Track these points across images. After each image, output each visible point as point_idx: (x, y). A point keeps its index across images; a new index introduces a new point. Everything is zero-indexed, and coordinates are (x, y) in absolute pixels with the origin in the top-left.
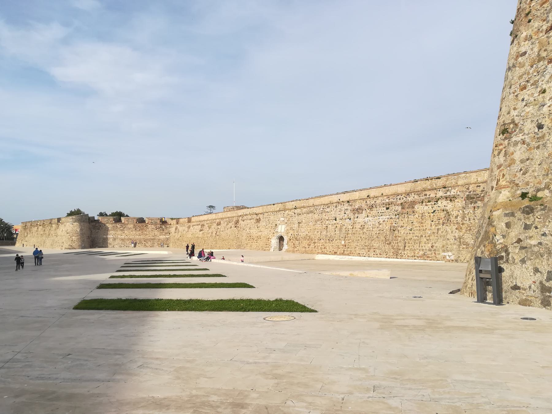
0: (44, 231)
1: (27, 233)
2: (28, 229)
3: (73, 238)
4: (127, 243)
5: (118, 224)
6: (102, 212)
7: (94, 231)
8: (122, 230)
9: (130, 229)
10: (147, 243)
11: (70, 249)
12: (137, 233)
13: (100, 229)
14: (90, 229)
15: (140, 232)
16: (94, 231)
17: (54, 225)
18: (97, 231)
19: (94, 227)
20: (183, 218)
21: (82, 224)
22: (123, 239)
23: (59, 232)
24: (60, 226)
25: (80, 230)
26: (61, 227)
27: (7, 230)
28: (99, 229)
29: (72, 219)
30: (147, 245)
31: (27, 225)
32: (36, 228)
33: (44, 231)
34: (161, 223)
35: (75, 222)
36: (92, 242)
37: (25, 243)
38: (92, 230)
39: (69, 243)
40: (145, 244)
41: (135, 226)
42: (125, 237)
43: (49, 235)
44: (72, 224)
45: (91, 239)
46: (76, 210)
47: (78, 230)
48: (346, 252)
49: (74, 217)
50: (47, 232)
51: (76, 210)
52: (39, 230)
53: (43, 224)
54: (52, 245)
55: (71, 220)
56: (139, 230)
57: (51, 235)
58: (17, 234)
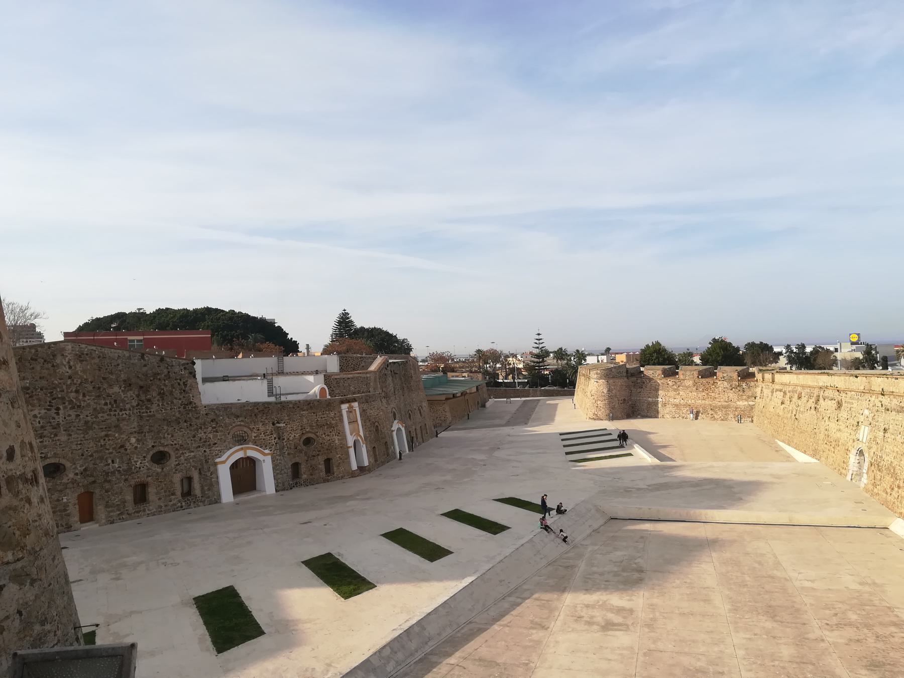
4: (684, 411)
5: (669, 380)
7: (634, 390)
8: (675, 390)
9: (688, 387)
12: (700, 395)
13: (644, 387)
14: (628, 387)
15: (704, 394)
16: (634, 390)
18: (639, 390)
19: (635, 384)
21: (611, 381)
22: (677, 405)
25: (608, 391)
30: (716, 416)
34: (739, 378)
35: (601, 378)
38: (632, 389)
39: (593, 411)
40: (712, 414)
41: (695, 384)
44: (597, 382)
46: (654, 343)
47: (605, 391)
51: (654, 343)
56: (703, 389)
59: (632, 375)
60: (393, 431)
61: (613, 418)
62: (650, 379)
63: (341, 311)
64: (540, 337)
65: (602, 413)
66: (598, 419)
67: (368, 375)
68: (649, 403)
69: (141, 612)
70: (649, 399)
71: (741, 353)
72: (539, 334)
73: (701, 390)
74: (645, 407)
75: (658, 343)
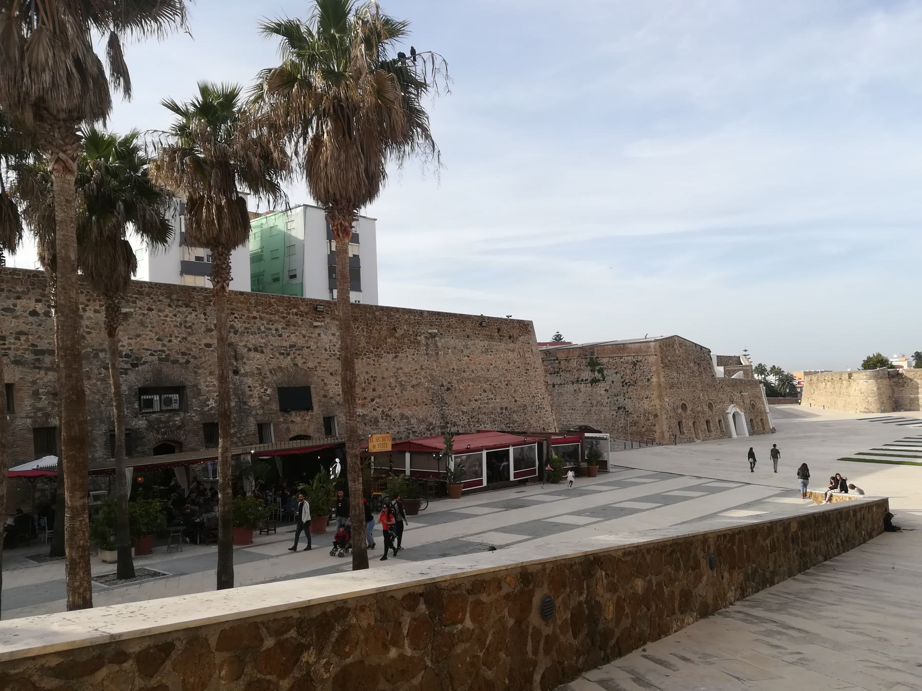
0: (834, 388)
1: (814, 390)
2: (815, 385)
6: (919, 351)
11: (867, 413)
13: (906, 386)
14: (891, 386)
16: (896, 389)
17: (844, 382)
18: (901, 388)
19: (897, 384)
20: (502, 543)
21: (879, 381)
23: (852, 392)
24: (852, 383)
25: (878, 389)
26: (854, 385)
27: (788, 383)
29: (866, 375)
31: (813, 379)
32: (824, 383)
33: (834, 388)
35: (870, 378)
36: (896, 403)
37: (812, 402)
38: (894, 388)
39: (864, 406)
43: (840, 394)
45: (893, 399)
46: (875, 355)
47: (875, 389)
48: (434, 435)
49: (868, 373)
50: (837, 390)
51: (875, 355)
52: (828, 386)
53: (832, 379)
54: (844, 406)
55: (865, 377)
57: (842, 393)
58: (801, 388)
59: (893, 377)
60: (728, 413)
61: (883, 411)
62: (911, 380)
63: (555, 333)
64: (747, 353)
65: (873, 407)
66: (869, 412)
67: (748, 368)
68: (911, 399)
69: (776, 472)
70: (912, 396)
71: (198, 520)
72: (746, 351)
74: (907, 402)
75: (879, 355)
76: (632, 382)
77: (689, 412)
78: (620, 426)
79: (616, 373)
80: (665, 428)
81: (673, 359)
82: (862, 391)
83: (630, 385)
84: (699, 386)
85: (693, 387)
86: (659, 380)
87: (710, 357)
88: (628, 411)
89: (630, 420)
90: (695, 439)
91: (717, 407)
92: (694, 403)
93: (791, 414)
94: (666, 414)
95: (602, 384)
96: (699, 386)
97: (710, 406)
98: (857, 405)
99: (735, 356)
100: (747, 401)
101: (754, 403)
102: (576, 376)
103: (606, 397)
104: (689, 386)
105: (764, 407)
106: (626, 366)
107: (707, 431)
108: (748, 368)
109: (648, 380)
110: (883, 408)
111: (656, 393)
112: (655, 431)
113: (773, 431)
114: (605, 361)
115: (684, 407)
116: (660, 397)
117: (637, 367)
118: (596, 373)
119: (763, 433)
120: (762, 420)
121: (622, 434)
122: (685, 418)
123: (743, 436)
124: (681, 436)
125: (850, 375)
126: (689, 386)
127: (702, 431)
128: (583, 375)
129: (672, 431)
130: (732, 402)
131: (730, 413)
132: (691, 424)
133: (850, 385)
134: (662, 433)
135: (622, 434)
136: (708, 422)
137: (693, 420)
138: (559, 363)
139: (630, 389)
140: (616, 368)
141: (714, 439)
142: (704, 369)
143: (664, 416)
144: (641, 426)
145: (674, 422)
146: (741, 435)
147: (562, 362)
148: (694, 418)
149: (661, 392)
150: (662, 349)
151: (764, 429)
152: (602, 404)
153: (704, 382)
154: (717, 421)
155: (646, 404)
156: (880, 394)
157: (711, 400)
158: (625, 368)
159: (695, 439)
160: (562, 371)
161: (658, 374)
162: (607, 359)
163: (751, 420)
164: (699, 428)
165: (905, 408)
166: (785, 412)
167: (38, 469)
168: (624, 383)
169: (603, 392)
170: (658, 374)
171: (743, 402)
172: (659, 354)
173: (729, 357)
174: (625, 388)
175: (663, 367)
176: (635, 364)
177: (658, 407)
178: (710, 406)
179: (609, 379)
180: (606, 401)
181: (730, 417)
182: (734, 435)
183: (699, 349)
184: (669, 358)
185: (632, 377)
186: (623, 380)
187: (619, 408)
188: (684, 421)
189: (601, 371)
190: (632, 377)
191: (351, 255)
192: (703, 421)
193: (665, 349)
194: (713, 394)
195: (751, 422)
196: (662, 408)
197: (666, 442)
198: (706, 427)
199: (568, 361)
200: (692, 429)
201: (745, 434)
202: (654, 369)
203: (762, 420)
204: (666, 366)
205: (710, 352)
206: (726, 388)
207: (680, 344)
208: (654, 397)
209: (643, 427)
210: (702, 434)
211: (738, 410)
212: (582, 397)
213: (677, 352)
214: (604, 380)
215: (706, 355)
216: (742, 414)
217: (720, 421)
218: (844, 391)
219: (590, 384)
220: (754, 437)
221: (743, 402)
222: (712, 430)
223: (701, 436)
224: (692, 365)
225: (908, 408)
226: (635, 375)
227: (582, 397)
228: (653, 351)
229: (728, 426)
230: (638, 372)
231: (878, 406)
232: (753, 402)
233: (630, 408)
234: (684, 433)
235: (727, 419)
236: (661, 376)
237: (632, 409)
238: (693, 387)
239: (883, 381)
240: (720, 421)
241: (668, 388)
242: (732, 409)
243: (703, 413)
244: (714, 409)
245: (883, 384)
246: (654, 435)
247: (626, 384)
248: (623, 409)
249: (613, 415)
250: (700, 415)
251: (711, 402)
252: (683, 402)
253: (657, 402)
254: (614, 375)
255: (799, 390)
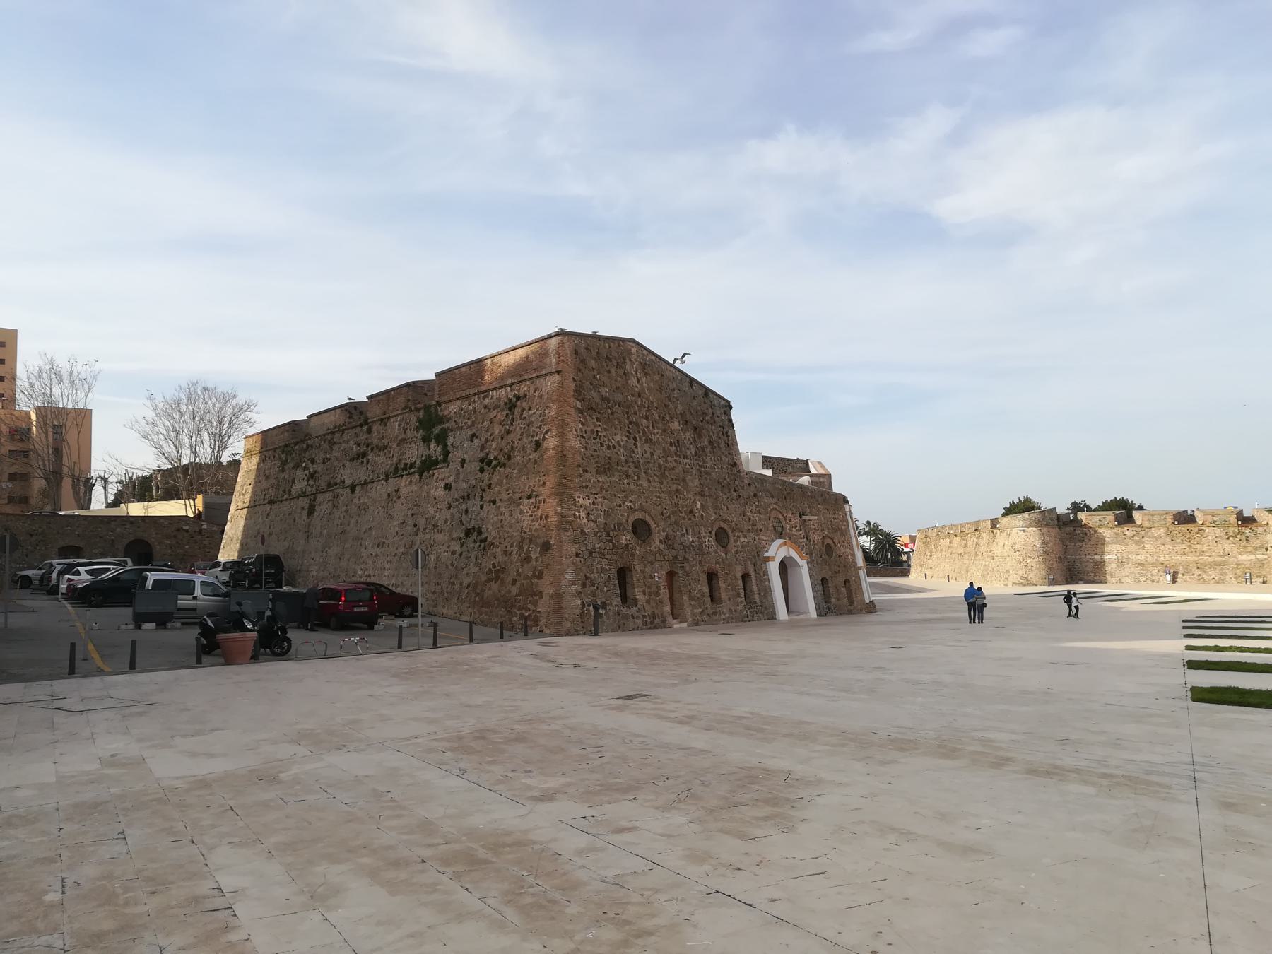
1: (931, 552)
2: (932, 544)
3: (1029, 561)
8: (1137, 543)
10: (1205, 572)
14: (1062, 540)
15: (1184, 546)
16: (1070, 545)
17: (984, 535)
18: (1079, 544)
19: (1072, 537)
21: (1045, 530)
23: (998, 548)
26: (1001, 537)
28: (1083, 541)
35: (1030, 525)
36: (1070, 570)
37: (929, 572)
38: (1068, 543)
39: (1021, 573)
40: (1199, 575)
42: (1147, 558)
43: (976, 555)
44: (1024, 531)
46: (1022, 499)
47: (1038, 543)
49: (1027, 516)
50: (970, 549)
51: (1022, 499)
52: (955, 544)
53: (962, 532)
55: (1021, 522)
60: (768, 559)
65: (1037, 573)
73: (1179, 541)
76: (501, 459)
77: (656, 543)
78: (466, 581)
79: (473, 437)
80: (569, 582)
81: (619, 397)
82: (1016, 547)
83: (496, 466)
84: (694, 483)
85: (676, 480)
86: (562, 442)
87: (730, 420)
88: (486, 539)
89: (487, 563)
90: (670, 619)
91: (739, 542)
92: (676, 523)
93: (902, 589)
94: (574, 541)
95: (441, 473)
96: (694, 483)
97: (721, 537)
98: (1008, 571)
99: (798, 460)
100: (817, 537)
101: (831, 542)
102: (395, 459)
103: (445, 505)
104: (663, 476)
105: (853, 555)
106: (492, 415)
107: (707, 599)
108: (822, 480)
109: (538, 445)
110: (1051, 577)
111: (551, 481)
112: (540, 594)
113: (871, 608)
114: (452, 409)
115: (641, 530)
116: (563, 491)
117: (517, 411)
118: (433, 445)
119: (850, 612)
120: (847, 581)
121: (466, 604)
122: (642, 559)
123: (801, 617)
124: (624, 610)
125: (994, 523)
126: (663, 476)
127: (691, 599)
128: (408, 453)
129: (593, 594)
130: (781, 535)
131: (773, 559)
132: (659, 577)
133: (994, 539)
134: (558, 597)
135: (466, 604)
136: (711, 577)
137: (667, 568)
138: (369, 431)
139: (496, 478)
140: (473, 425)
141: (726, 621)
142: (710, 442)
143: (570, 549)
144: (509, 580)
145: (604, 570)
146: (799, 613)
147: (375, 428)
148: (670, 562)
149: (564, 476)
150: (583, 361)
151: (852, 603)
152: (435, 526)
153: (707, 473)
154: (739, 576)
155: (526, 516)
156: (1047, 553)
157: (724, 521)
158: (491, 421)
159: (670, 619)
160: (372, 450)
161: (562, 427)
162: (458, 403)
163: (824, 581)
164: (685, 590)
165: (1085, 577)
166: (885, 585)
167: (1107, 650)
168: (485, 462)
169: (440, 493)
170: (562, 427)
171: (807, 537)
172: (570, 371)
173: (788, 460)
174: (486, 476)
175: (580, 411)
176: (511, 406)
177: (553, 520)
178: (721, 537)
179: (455, 456)
180: (446, 514)
181: (773, 569)
182: (782, 613)
183: (701, 393)
184: (605, 391)
185: (503, 445)
186: (483, 455)
187: (468, 533)
188: (638, 567)
189: (442, 439)
190: (503, 444)
191: (367, 400)
192: (699, 572)
193: (593, 364)
194: (732, 507)
195: (822, 586)
196: (565, 522)
197: (569, 625)
198: (706, 590)
199: (385, 425)
200: (664, 594)
201: (807, 612)
202: (552, 414)
203: (847, 581)
204: (589, 409)
205: (731, 407)
206: (765, 500)
207: (644, 365)
208: (546, 491)
209: (514, 582)
210: (694, 607)
211: (793, 554)
212: (401, 510)
213: (633, 381)
214: (445, 460)
215: (718, 411)
216: (803, 563)
217: (745, 577)
218: (982, 549)
219: (417, 476)
220: (830, 619)
221: (807, 537)
222: (724, 596)
223: (688, 611)
224: (676, 426)
225: (1090, 578)
226: (511, 436)
227: (401, 510)
228: (554, 361)
229: (766, 591)
230: (518, 427)
231: (1044, 573)
232: (828, 541)
233: (490, 533)
234: (636, 602)
235: (766, 572)
236: (571, 434)
237: (494, 533)
238: (676, 480)
239: (1050, 529)
240: (745, 577)
241: (592, 469)
242: (778, 551)
243: (701, 551)
244: (732, 547)
245: (1050, 537)
246: (535, 604)
247: (489, 464)
248: (476, 533)
249: (453, 553)
250: (691, 556)
251: (725, 526)
252: (639, 515)
253: (551, 506)
254: (467, 444)
255: (904, 558)
